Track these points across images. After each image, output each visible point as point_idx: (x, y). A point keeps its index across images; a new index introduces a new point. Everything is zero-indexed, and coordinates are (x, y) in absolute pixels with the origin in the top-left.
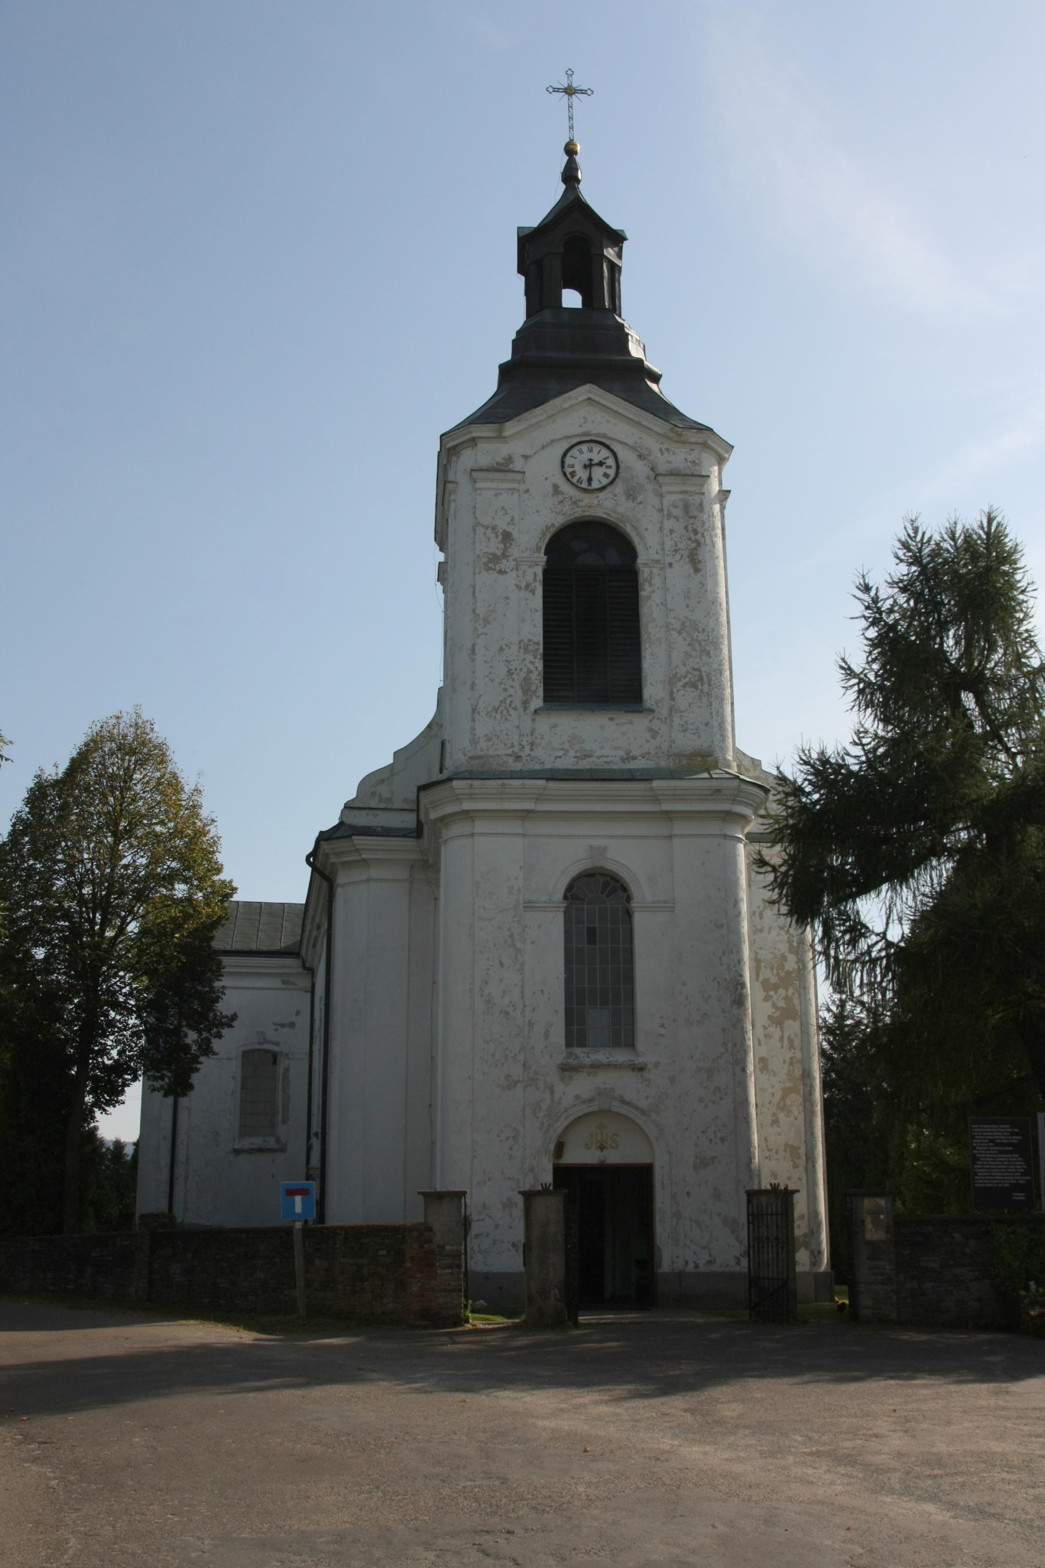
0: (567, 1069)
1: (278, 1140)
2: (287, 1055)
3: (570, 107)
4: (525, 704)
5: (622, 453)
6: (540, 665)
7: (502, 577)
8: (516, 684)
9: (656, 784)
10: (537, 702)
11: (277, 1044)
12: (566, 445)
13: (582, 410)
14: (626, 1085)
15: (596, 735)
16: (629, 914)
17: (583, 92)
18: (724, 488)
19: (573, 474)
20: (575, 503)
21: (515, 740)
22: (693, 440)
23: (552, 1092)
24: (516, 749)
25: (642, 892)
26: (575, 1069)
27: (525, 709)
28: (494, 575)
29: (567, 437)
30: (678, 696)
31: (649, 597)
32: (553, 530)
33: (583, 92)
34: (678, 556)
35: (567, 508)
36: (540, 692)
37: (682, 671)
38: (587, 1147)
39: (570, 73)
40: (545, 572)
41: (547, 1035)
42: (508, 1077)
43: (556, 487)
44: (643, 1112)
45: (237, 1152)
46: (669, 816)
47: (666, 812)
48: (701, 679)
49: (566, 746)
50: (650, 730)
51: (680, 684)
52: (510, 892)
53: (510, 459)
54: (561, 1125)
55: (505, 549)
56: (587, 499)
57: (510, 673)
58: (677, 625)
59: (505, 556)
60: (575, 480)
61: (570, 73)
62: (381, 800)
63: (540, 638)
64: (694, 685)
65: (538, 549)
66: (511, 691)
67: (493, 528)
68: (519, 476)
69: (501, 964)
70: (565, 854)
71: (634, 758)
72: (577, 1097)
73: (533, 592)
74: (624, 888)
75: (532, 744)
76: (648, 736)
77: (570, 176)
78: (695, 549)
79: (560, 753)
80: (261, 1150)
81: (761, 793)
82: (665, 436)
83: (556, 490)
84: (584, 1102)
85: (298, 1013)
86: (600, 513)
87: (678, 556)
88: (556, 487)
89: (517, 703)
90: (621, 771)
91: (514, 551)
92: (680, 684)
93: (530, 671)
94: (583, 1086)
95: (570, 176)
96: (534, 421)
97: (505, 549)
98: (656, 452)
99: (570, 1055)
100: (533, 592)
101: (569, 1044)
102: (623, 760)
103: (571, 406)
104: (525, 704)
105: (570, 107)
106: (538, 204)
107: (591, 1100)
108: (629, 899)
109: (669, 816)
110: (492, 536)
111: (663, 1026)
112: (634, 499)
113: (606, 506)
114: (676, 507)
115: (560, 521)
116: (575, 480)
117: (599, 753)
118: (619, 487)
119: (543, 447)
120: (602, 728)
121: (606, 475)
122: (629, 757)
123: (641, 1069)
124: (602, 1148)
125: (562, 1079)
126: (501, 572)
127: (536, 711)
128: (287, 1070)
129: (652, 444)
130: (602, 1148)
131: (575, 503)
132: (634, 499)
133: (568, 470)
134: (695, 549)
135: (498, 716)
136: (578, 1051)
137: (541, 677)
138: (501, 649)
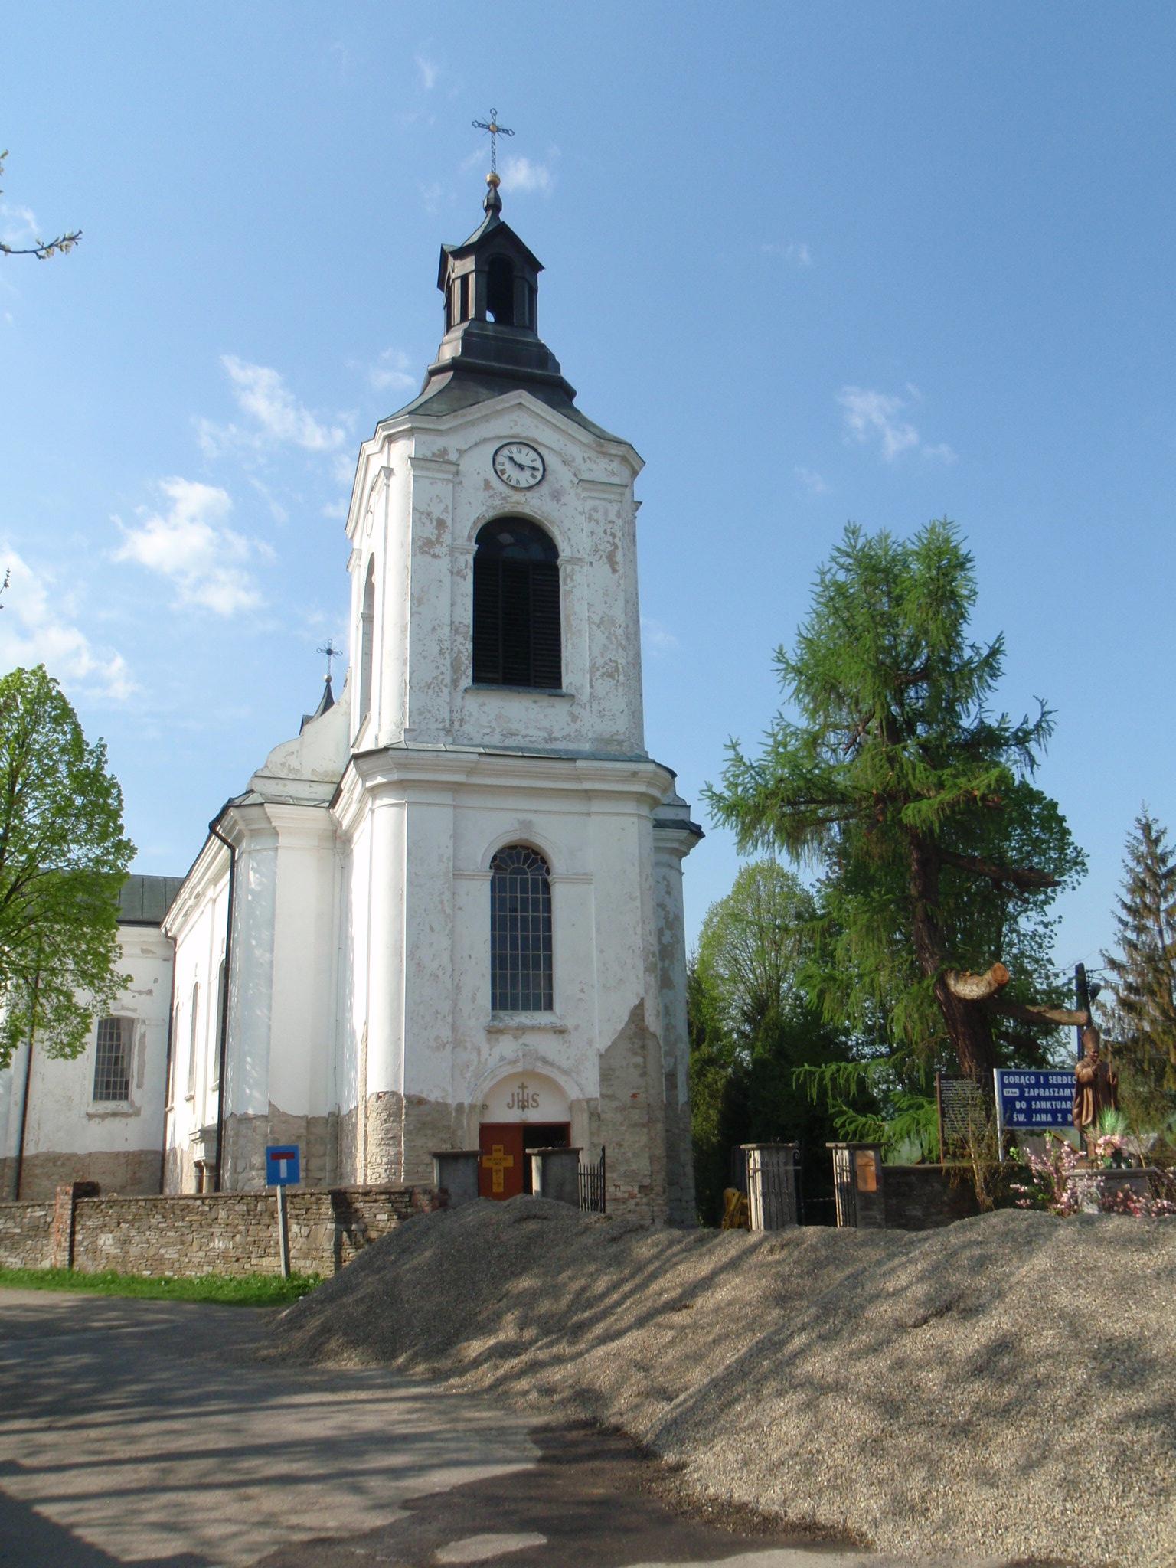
0: (493, 1032)
1: (132, 1105)
2: (144, 1022)
3: (493, 143)
4: (455, 682)
5: (551, 460)
6: (470, 647)
7: (436, 561)
8: (448, 662)
9: (580, 764)
10: (467, 681)
11: (135, 1010)
12: (505, 441)
13: (520, 414)
14: (548, 1046)
15: (519, 714)
16: (547, 887)
17: (505, 131)
18: (636, 499)
19: (503, 472)
20: (504, 498)
21: (447, 716)
22: (613, 452)
23: (479, 1054)
24: (447, 724)
25: (558, 864)
26: (500, 1031)
27: (456, 687)
28: (429, 558)
29: (499, 438)
30: (597, 684)
31: (570, 592)
32: (483, 522)
33: (505, 131)
34: (597, 557)
35: (497, 502)
36: (470, 672)
37: (600, 661)
38: (510, 1107)
39: (494, 113)
40: (476, 560)
41: (474, 999)
42: (437, 1037)
43: (487, 483)
44: (566, 1072)
45: (90, 1116)
46: (588, 795)
47: (586, 791)
48: (617, 670)
49: (494, 724)
50: (571, 714)
51: (598, 673)
52: (441, 861)
53: (445, 451)
54: (487, 1085)
55: (439, 536)
56: (517, 497)
57: (441, 652)
58: (597, 619)
59: (439, 541)
60: (505, 477)
61: (494, 113)
62: (290, 771)
63: (470, 621)
64: (611, 676)
65: (469, 538)
66: (443, 669)
67: (428, 514)
68: (453, 468)
69: (432, 929)
70: (493, 827)
71: (556, 739)
72: (503, 1058)
73: (464, 578)
74: (544, 861)
75: (462, 720)
76: (569, 719)
77: (494, 206)
78: (613, 551)
79: (488, 731)
80: (114, 1115)
81: (668, 776)
82: (588, 446)
83: (487, 485)
84: (509, 1063)
85: (156, 981)
86: (527, 510)
87: (597, 557)
88: (487, 483)
89: (448, 680)
90: (546, 751)
91: (447, 537)
92: (598, 673)
93: (460, 652)
94: (507, 1046)
95: (494, 206)
96: (469, 418)
97: (439, 536)
98: (579, 460)
99: (494, 1018)
100: (464, 578)
101: (494, 1007)
102: (546, 741)
103: (503, 409)
104: (455, 682)
105: (493, 143)
106: (471, 227)
107: (515, 1062)
108: (548, 872)
109: (588, 795)
110: (427, 522)
111: (582, 991)
112: (558, 501)
113: (533, 505)
114: (596, 511)
115: (491, 514)
116: (505, 477)
117: (523, 732)
118: (545, 489)
119: (477, 444)
120: (527, 709)
121: (534, 477)
122: (551, 739)
123: (560, 1031)
124: (523, 1107)
125: (489, 1041)
126: (434, 556)
127: (466, 690)
128: (143, 1036)
129: (575, 452)
130: (523, 1107)
131: (504, 498)
132: (558, 501)
133: (499, 468)
134: (613, 551)
135: (430, 691)
136: (502, 1013)
137: (471, 658)
138: (434, 629)
